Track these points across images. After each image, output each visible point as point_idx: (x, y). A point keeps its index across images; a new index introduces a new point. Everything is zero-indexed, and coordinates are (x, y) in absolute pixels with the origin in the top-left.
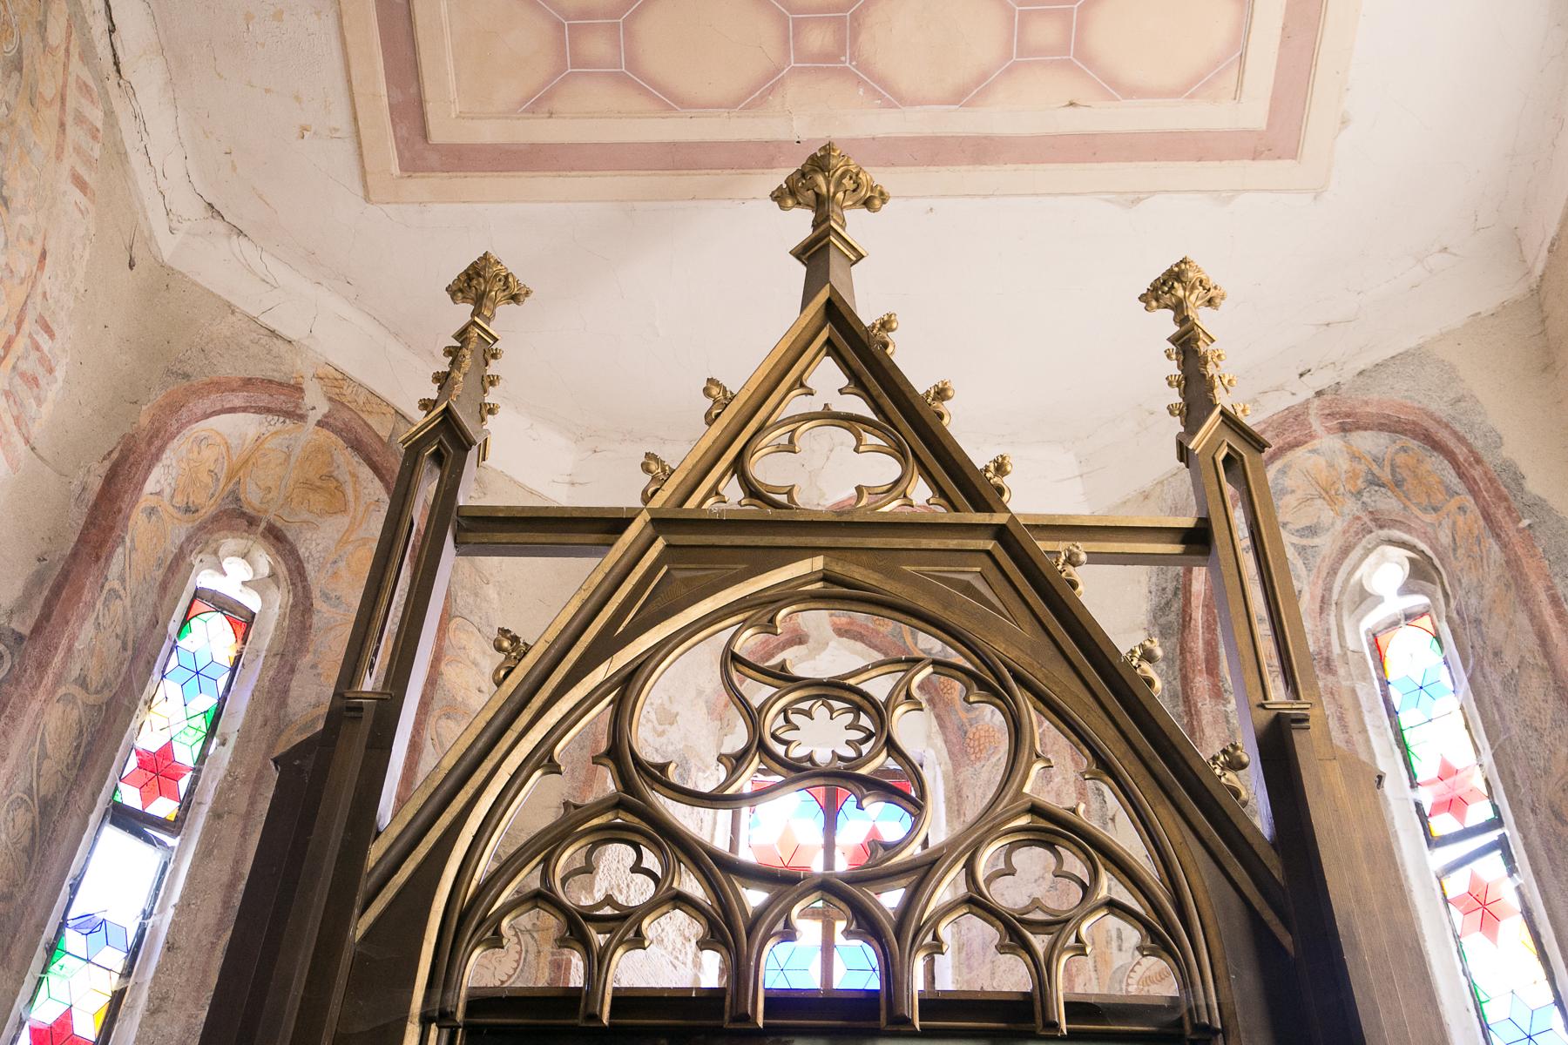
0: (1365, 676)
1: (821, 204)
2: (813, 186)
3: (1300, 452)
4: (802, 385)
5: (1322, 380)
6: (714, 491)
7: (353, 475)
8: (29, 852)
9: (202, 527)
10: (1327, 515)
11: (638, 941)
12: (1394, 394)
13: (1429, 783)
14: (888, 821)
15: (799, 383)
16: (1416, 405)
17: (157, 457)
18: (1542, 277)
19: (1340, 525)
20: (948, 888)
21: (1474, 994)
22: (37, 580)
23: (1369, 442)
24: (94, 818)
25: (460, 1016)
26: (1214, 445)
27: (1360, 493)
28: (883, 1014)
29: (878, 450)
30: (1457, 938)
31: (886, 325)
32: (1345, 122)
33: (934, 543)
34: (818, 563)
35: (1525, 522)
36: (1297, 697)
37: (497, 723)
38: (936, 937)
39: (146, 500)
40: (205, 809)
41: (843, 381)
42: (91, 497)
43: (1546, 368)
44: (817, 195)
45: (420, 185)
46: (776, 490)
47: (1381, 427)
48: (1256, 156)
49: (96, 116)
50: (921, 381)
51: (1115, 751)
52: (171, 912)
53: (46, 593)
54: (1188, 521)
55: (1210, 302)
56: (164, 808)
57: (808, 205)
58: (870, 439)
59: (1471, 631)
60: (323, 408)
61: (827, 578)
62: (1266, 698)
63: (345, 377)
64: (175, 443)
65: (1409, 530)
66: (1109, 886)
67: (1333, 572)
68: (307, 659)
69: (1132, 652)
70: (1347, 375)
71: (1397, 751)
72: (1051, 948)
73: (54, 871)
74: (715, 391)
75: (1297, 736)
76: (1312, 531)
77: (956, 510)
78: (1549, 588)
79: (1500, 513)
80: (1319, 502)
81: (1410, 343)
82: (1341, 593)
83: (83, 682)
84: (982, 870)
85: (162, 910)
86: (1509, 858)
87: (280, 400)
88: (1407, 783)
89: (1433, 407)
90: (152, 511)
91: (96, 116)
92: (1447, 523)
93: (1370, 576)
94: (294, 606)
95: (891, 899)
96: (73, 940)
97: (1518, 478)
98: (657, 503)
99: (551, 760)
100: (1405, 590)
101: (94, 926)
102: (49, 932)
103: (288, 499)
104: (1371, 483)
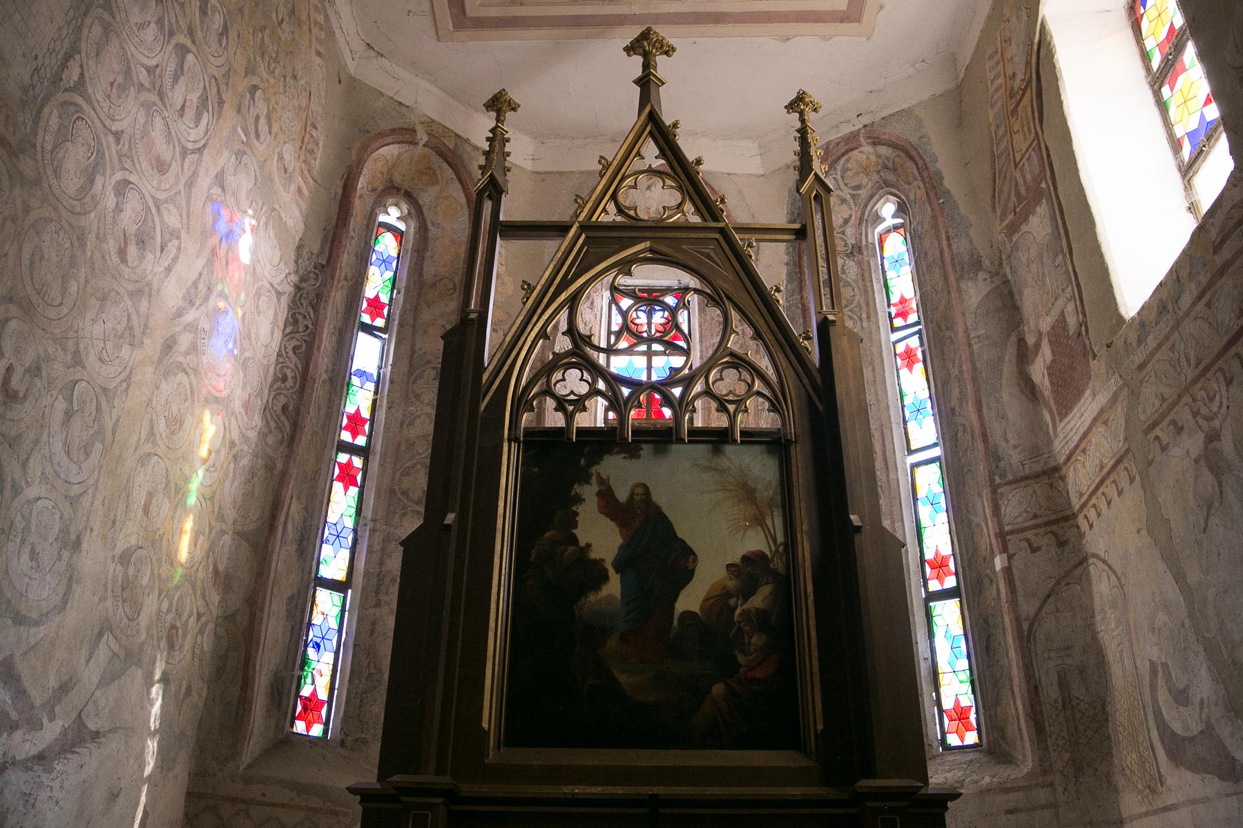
0: (875, 255)
1: (647, 56)
2: (642, 47)
3: (855, 152)
4: (640, 155)
5: (866, 120)
6: (604, 210)
7: (440, 167)
8: (337, 351)
9: (379, 196)
10: (865, 180)
11: (584, 409)
12: (897, 130)
13: (895, 305)
14: (678, 361)
15: (638, 154)
16: (905, 137)
17: (361, 173)
18: (962, 80)
19: (870, 185)
20: (698, 388)
21: (901, 393)
22: (325, 239)
23: (883, 150)
24: (355, 331)
25: (522, 439)
26: (810, 190)
27: (879, 171)
28: (674, 437)
29: (672, 187)
30: (898, 370)
31: (675, 125)
32: (881, 8)
33: (695, 235)
34: (648, 244)
35: (942, 200)
36: (834, 309)
37: (525, 320)
38: (694, 407)
39: (359, 192)
40: (396, 323)
41: (657, 152)
42: (339, 198)
43: (960, 125)
44: (644, 50)
45: (461, 34)
46: (629, 209)
47: (889, 146)
48: (842, 21)
49: (321, 19)
50: (691, 157)
51: (763, 329)
52: (390, 367)
53: (329, 245)
54: (797, 226)
55: (815, 110)
56: (380, 322)
57: (640, 55)
58: (669, 182)
59: (917, 241)
60: (425, 139)
61: (651, 250)
62: (822, 309)
63: (433, 121)
64: (366, 164)
65: (899, 190)
66: (758, 385)
67: (866, 206)
68: (429, 254)
69: (772, 288)
70: (877, 118)
71: (884, 289)
72: (735, 411)
73: (345, 356)
74: (603, 161)
75: (831, 329)
76: (858, 187)
77: (705, 221)
78: (946, 232)
79: (932, 195)
80: (862, 174)
81: (904, 106)
82: (868, 216)
83: (346, 279)
84: (711, 380)
85: (386, 366)
86: (921, 339)
87: (407, 137)
88: (886, 304)
89: (911, 139)
90: (361, 196)
91: (321, 19)
92: (913, 191)
93: (881, 208)
94: (420, 227)
95: (677, 391)
96: (355, 380)
97: (941, 178)
98: (581, 218)
99: (546, 334)
100: (894, 216)
101: (361, 374)
102: (347, 379)
103: (413, 179)
104: (885, 168)
